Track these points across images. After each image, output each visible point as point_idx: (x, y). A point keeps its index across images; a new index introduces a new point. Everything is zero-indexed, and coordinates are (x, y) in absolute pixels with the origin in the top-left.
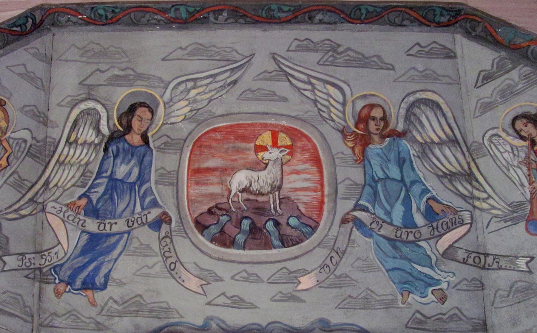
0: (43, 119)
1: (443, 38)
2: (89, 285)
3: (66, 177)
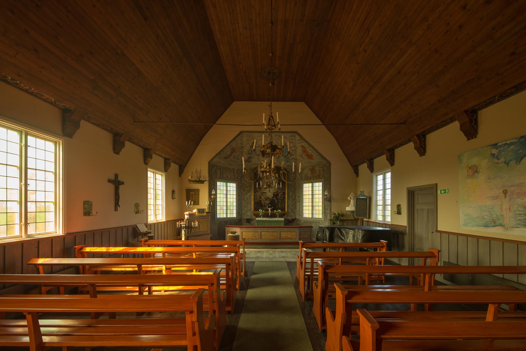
0: (242, 144)
1: (294, 134)
2: (249, 162)
3: (246, 150)
